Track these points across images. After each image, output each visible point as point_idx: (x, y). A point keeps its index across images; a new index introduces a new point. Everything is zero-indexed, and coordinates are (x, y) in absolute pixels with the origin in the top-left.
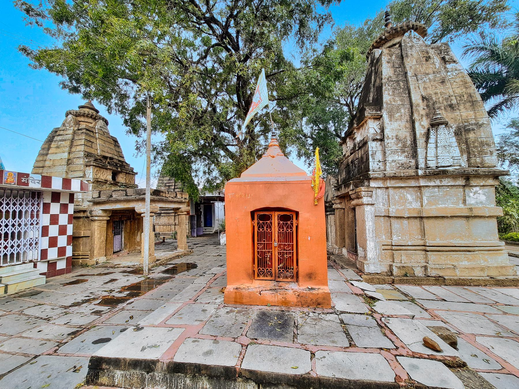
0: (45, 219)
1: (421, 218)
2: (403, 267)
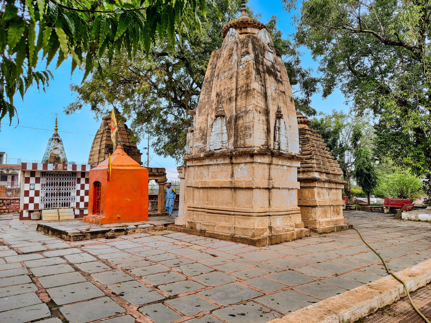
0: (78, 187)
1: (235, 189)
2: (191, 222)
